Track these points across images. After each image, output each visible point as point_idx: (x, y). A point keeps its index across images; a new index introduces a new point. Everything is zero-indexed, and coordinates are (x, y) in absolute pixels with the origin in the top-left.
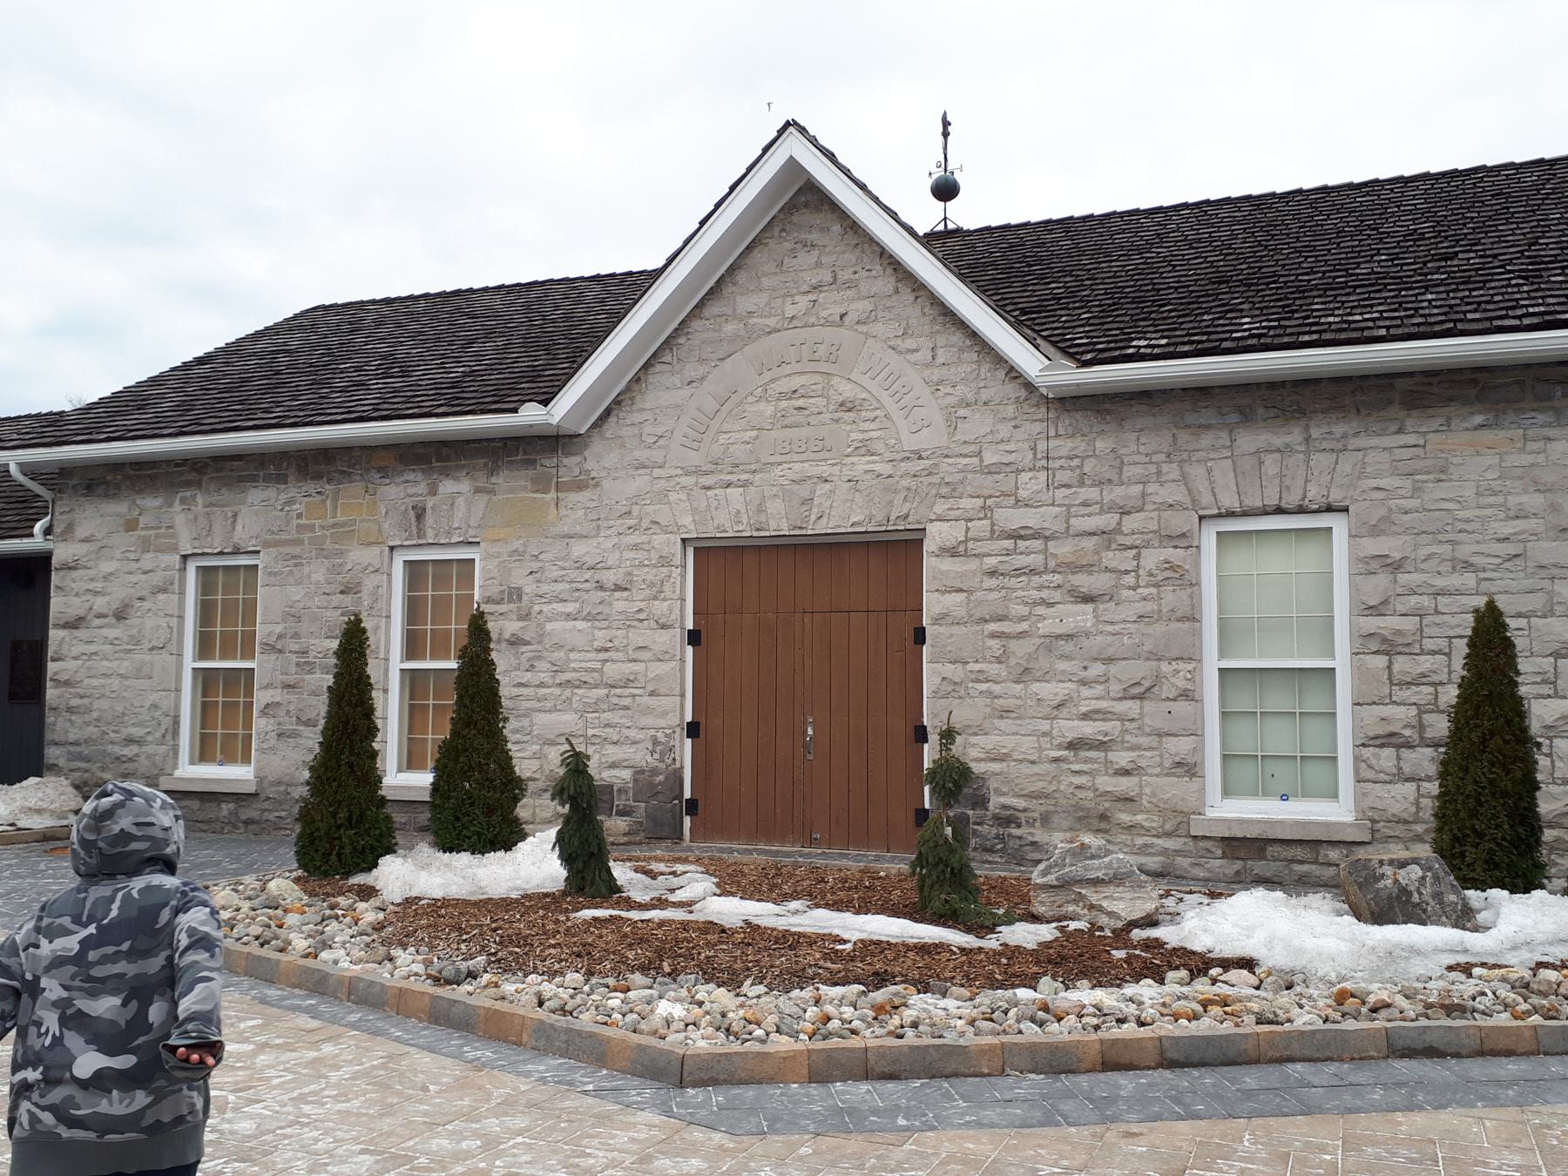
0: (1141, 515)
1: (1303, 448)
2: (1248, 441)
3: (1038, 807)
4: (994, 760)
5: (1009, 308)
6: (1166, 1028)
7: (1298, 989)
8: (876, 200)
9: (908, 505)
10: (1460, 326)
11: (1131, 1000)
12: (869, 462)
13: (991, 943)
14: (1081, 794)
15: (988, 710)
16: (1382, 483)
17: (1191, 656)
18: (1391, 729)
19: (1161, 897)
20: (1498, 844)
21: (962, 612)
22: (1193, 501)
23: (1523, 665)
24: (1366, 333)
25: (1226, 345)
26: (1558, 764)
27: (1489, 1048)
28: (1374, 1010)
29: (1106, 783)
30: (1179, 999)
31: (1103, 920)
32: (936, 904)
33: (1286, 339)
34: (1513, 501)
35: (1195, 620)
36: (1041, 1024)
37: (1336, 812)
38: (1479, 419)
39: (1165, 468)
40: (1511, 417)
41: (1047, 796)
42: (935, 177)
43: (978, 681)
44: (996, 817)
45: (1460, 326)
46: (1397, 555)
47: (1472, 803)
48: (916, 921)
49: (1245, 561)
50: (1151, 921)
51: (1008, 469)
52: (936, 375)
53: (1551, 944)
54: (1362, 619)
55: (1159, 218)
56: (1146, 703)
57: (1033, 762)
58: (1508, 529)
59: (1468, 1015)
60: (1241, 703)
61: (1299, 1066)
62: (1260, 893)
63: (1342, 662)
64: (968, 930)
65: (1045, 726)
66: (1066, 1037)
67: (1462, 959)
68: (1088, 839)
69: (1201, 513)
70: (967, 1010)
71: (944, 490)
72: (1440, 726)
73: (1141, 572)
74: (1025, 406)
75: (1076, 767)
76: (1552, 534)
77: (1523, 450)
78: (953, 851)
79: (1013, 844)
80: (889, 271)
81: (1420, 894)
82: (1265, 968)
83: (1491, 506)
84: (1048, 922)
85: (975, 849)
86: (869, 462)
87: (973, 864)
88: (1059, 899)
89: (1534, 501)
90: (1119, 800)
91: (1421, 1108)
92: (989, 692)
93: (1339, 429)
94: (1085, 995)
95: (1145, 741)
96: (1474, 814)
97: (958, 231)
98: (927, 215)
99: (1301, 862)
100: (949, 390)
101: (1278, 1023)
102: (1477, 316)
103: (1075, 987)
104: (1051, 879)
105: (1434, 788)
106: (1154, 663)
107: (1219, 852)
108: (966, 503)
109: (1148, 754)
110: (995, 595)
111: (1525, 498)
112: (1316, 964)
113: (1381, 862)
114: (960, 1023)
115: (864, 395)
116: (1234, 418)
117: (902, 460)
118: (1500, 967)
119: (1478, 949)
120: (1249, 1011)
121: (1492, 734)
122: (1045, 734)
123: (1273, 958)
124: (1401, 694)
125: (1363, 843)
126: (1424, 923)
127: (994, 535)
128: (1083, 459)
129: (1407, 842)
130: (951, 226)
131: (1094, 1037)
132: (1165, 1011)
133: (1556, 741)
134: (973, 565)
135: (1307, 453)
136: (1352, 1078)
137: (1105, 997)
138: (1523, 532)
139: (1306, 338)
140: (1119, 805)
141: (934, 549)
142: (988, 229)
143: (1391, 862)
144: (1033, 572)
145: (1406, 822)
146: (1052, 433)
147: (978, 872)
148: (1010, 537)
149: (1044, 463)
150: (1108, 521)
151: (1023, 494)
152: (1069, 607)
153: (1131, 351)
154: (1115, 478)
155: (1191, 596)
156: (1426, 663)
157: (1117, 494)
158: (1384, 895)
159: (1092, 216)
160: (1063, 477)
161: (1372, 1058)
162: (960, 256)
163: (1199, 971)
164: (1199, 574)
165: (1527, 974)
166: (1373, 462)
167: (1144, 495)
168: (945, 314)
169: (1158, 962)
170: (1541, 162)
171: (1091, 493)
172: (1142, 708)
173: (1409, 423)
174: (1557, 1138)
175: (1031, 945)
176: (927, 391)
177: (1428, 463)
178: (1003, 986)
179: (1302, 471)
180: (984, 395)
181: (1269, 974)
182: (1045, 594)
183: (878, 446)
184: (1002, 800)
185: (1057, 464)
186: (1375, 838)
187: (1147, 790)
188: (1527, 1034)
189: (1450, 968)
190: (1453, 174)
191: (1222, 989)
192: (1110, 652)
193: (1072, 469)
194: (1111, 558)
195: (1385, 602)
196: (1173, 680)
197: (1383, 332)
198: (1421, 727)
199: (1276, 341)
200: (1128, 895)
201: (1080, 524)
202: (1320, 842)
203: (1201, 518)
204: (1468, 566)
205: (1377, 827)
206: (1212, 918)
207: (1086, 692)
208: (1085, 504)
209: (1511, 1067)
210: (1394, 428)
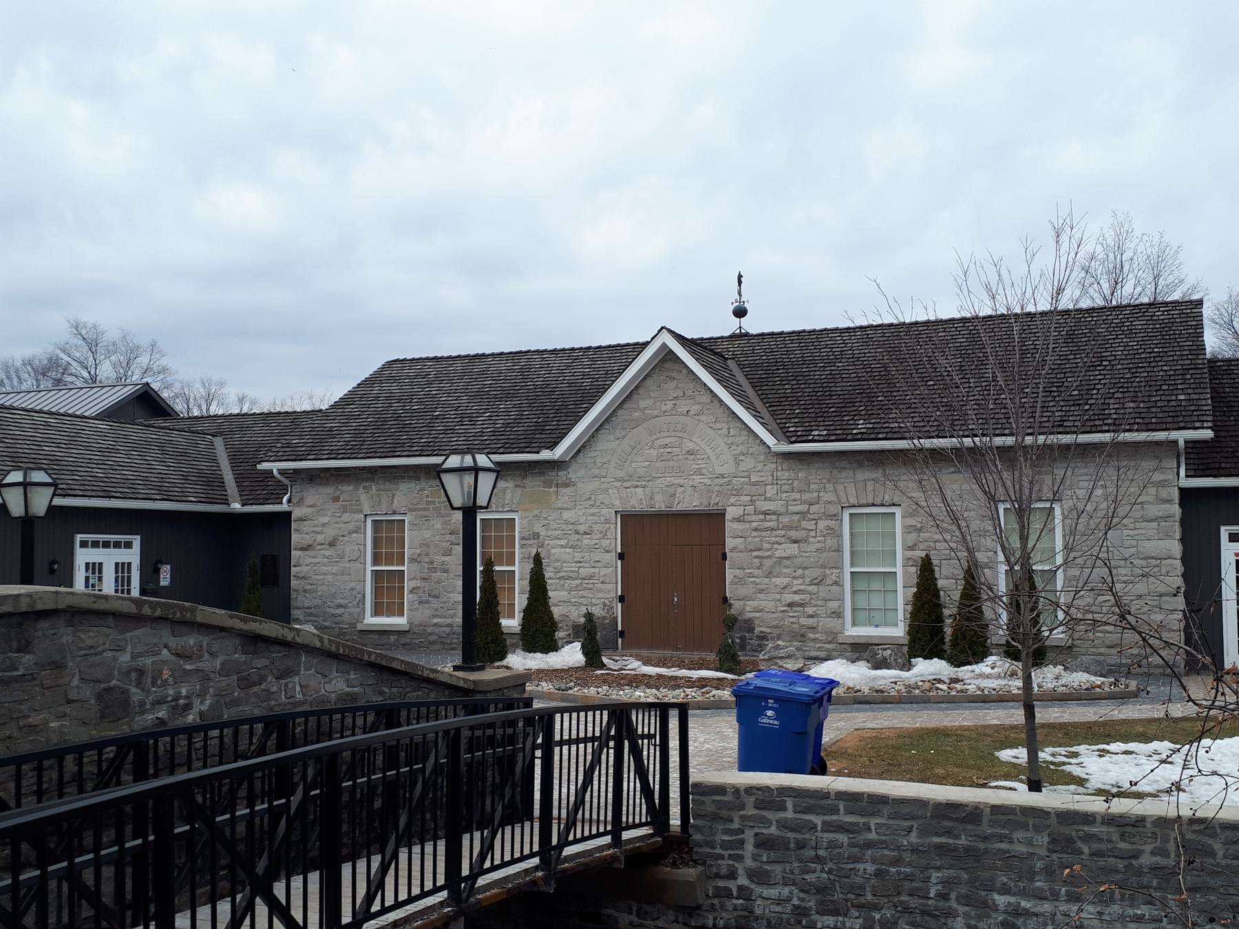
2: (861, 475)
17: (840, 567)
29: (803, 621)
49: (863, 527)
60: (862, 585)
63: (899, 569)
150: (804, 508)
157: (806, 496)
171: (797, 496)
194: (804, 524)
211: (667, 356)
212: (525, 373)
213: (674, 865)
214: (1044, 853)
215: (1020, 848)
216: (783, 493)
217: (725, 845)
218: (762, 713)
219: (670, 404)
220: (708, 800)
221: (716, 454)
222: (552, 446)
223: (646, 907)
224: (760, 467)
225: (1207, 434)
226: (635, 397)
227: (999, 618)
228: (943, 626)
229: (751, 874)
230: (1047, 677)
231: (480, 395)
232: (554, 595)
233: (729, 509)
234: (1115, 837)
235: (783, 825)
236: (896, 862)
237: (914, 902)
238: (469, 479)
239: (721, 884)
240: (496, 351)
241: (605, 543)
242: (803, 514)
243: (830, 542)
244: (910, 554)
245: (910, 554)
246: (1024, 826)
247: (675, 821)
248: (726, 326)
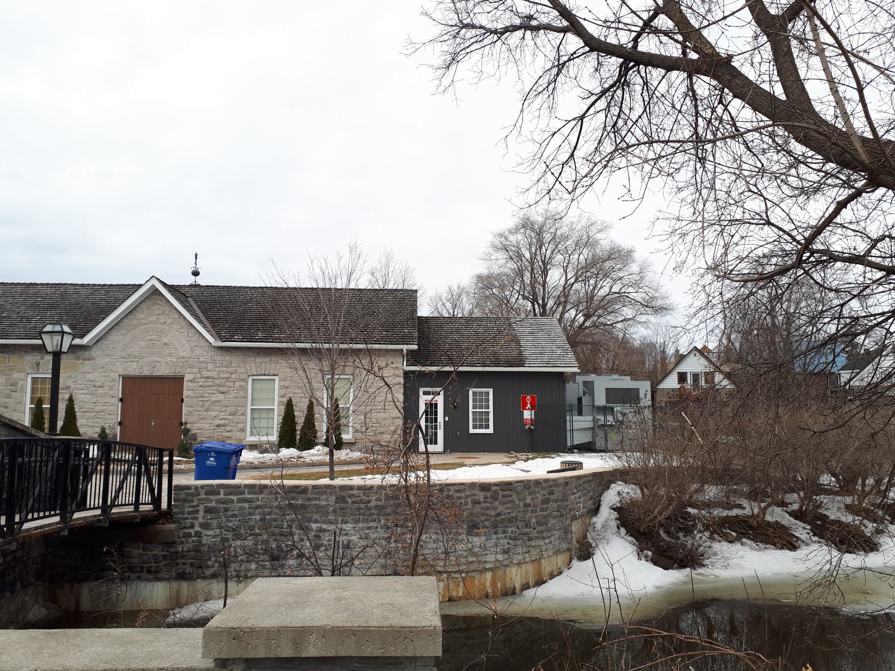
2: (259, 360)
17: (245, 406)
29: (225, 434)
49: (258, 386)
60: (256, 415)
63: (276, 407)
108: (195, 370)
157: (230, 370)
171: (225, 369)
194: (228, 384)
211: (155, 292)
212: (64, 296)
213: (163, 524)
214: (333, 504)
215: (323, 503)
216: (218, 367)
217: (189, 513)
218: (208, 459)
219: (155, 318)
220: (182, 493)
221: (180, 346)
222: (82, 336)
223: (147, 545)
224: (205, 353)
225: (415, 347)
226: (134, 312)
227: (322, 427)
228: (295, 433)
229: (202, 525)
230: (342, 455)
231: (33, 306)
232: (80, 422)
233: (186, 375)
234: (362, 495)
235: (219, 501)
236: (269, 514)
237: (276, 531)
238: (57, 338)
239: (186, 531)
240: (44, 282)
241: (112, 392)
242: (228, 379)
243: (241, 393)
244: (282, 399)
245: (282, 399)
246: (325, 493)
247: (164, 505)
248: (189, 280)
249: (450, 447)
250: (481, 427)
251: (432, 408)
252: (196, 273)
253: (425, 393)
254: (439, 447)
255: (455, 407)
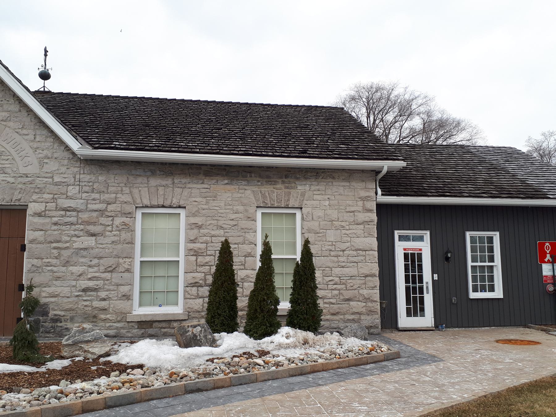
0: (115, 205)
1: (171, 186)
2: (154, 182)
3: (69, 314)
4: (52, 297)
5: (67, 124)
6: (108, 394)
7: (157, 374)
8: (12, 74)
9: (21, 195)
10: (221, 151)
11: (96, 385)
12: (4, 177)
13: (43, 369)
14: (87, 309)
15: (51, 277)
16: (197, 199)
17: (131, 257)
18: (196, 281)
19: (113, 345)
20: (225, 318)
21: (42, 239)
22: (134, 201)
23: (235, 259)
24: (193, 150)
25: (147, 148)
26: (245, 290)
27: (217, 386)
28: (182, 378)
29: (96, 304)
30: (114, 382)
31: (89, 356)
32: (20, 356)
33: (167, 149)
34: (235, 208)
35: (132, 243)
36: (59, 399)
37: (176, 310)
38: (226, 181)
39: (124, 189)
40: (235, 182)
41: (73, 310)
42: (40, 70)
43: (47, 266)
44: (52, 319)
45: (221, 151)
46: (200, 223)
47: (218, 304)
48: (11, 364)
49: (151, 223)
50: (108, 354)
51: (64, 184)
52: (35, 145)
53: (238, 349)
54: (189, 244)
55: (127, 100)
56: (113, 274)
57: (68, 297)
58: (233, 216)
59: (211, 376)
60: (148, 273)
61: (155, 402)
62: (147, 341)
63: (181, 259)
64: (33, 365)
65: (74, 283)
66: (69, 402)
67: (211, 357)
68: (85, 326)
69: (137, 205)
70: (28, 397)
71: (37, 190)
72: (210, 279)
73: (114, 226)
74: (72, 161)
75: (85, 298)
76: (245, 219)
77: (238, 192)
78: (29, 334)
79: (58, 329)
80: (17, 102)
81: (200, 336)
82: (146, 368)
83: (229, 209)
84: (68, 359)
85: (42, 332)
86: (4, 177)
87: (37, 339)
88: (72, 350)
89: (241, 208)
90: (101, 310)
91: (193, 410)
92: (52, 270)
93: (184, 181)
94: (79, 385)
95: (112, 288)
96: (218, 308)
97: (49, 92)
98: (36, 84)
99: (164, 328)
100: (41, 152)
101: (148, 387)
102: (226, 149)
103: (75, 383)
104: (70, 342)
105: (207, 300)
106: (117, 259)
107: (136, 327)
108: (46, 196)
109: (113, 292)
110: (56, 232)
111: (238, 207)
112: (164, 364)
113: (188, 326)
114: (24, 403)
115: (3, 150)
116: (149, 173)
117: (19, 177)
118: (222, 358)
119: (216, 353)
120: (139, 384)
121: (225, 282)
122: (74, 286)
123: (149, 363)
124: (199, 269)
125: (185, 320)
126: (200, 346)
127: (57, 209)
128: (94, 183)
129: (199, 318)
130: (46, 90)
131: (80, 401)
132: (109, 387)
133: (245, 284)
134: (47, 220)
135: (173, 188)
136: (172, 403)
137: (86, 385)
138: (237, 218)
139: (174, 149)
140: (101, 312)
141: (32, 213)
142: (62, 93)
143: (191, 326)
144: (72, 224)
145: (199, 312)
146: (82, 172)
147: (40, 342)
148: (63, 210)
149: (78, 183)
150: (102, 206)
151: (69, 194)
152: (86, 237)
153: (113, 146)
154: (106, 191)
155: (131, 235)
156: (208, 259)
157: (106, 197)
158: (188, 338)
159: (102, 95)
160: (86, 189)
161: (180, 395)
162: (49, 101)
163: (123, 371)
164: (135, 227)
165: (230, 360)
166: (194, 191)
167: (116, 198)
168: (40, 123)
169: (107, 369)
170: (247, 103)
171: (97, 196)
172: (111, 276)
173: (205, 180)
174: (233, 414)
175: (59, 368)
176: (31, 151)
177: (211, 194)
178: (45, 386)
179: (171, 194)
180: (55, 155)
181: (148, 369)
182: (76, 233)
183: (9, 171)
184: (55, 312)
185: (83, 184)
186: (189, 318)
187: (112, 306)
188: (228, 380)
189: (207, 361)
190: (222, 103)
191: (131, 377)
192: (101, 255)
193: (89, 186)
194: (103, 220)
195: (196, 239)
196: (123, 265)
197: (198, 150)
198: (205, 280)
199: (164, 149)
200: (100, 346)
201: (91, 207)
202: (171, 320)
203: (136, 207)
204: (222, 228)
205: (190, 314)
206: (130, 351)
207: (91, 270)
208: (94, 200)
209: (222, 392)
210: (201, 182)
242: (102, 212)
249: (444, 321)
250: (483, 289)
251: (413, 260)
252: (45, 76)
253: (401, 238)
254: (427, 319)
255: (447, 259)
